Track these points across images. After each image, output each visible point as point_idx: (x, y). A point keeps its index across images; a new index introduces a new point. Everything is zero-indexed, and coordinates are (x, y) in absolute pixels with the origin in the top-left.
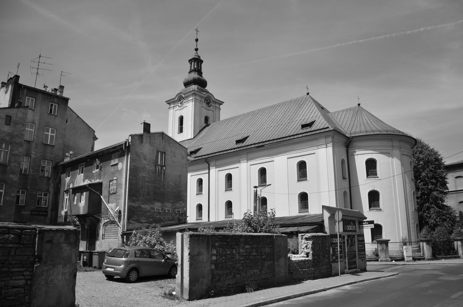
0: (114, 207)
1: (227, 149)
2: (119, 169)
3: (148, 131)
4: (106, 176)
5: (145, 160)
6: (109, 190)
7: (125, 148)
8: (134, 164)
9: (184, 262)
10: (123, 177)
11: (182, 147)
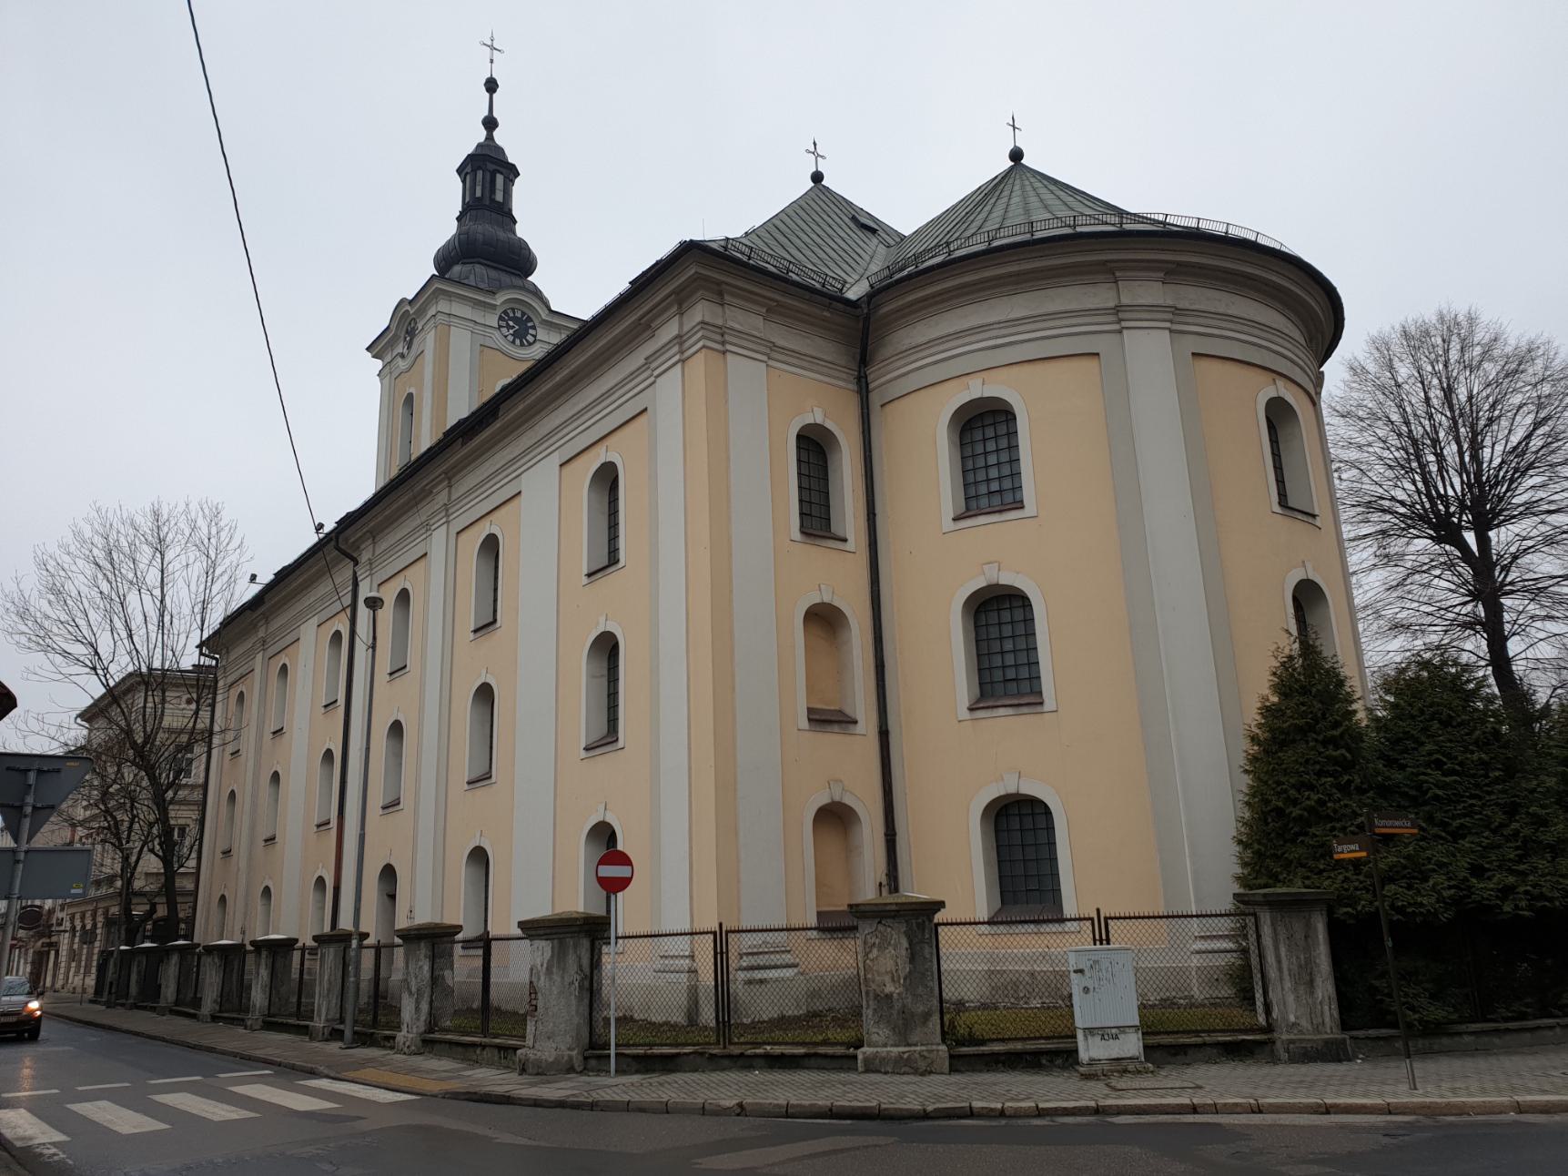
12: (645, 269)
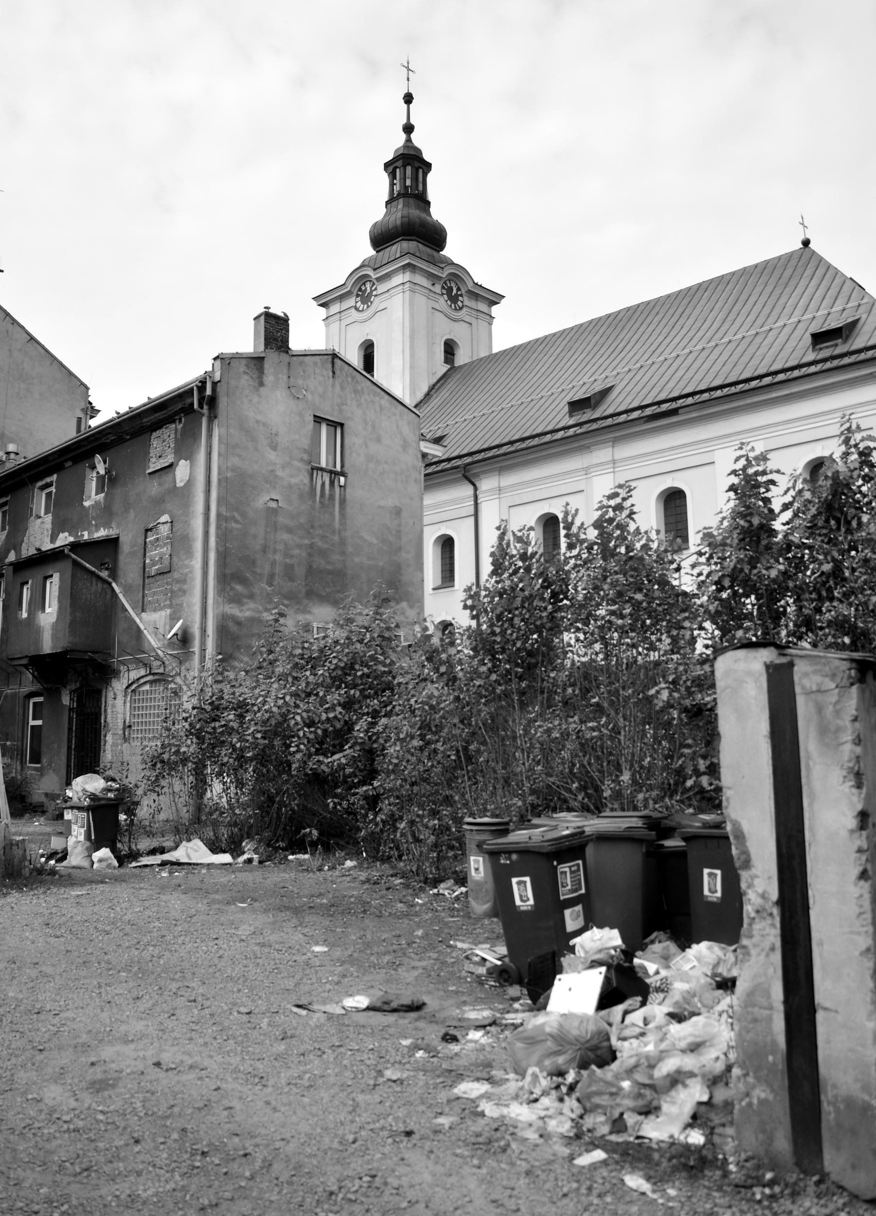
0: (165, 625)
1: (539, 430)
2: (178, 486)
3: (280, 344)
4: (132, 515)
5: (274, 448)
6: (144, 562)
7: (201, 406)
8: (235, 461)
9: (810, 879)
10: (193, 512)
11: (400, 407)
12: (812, 913)
